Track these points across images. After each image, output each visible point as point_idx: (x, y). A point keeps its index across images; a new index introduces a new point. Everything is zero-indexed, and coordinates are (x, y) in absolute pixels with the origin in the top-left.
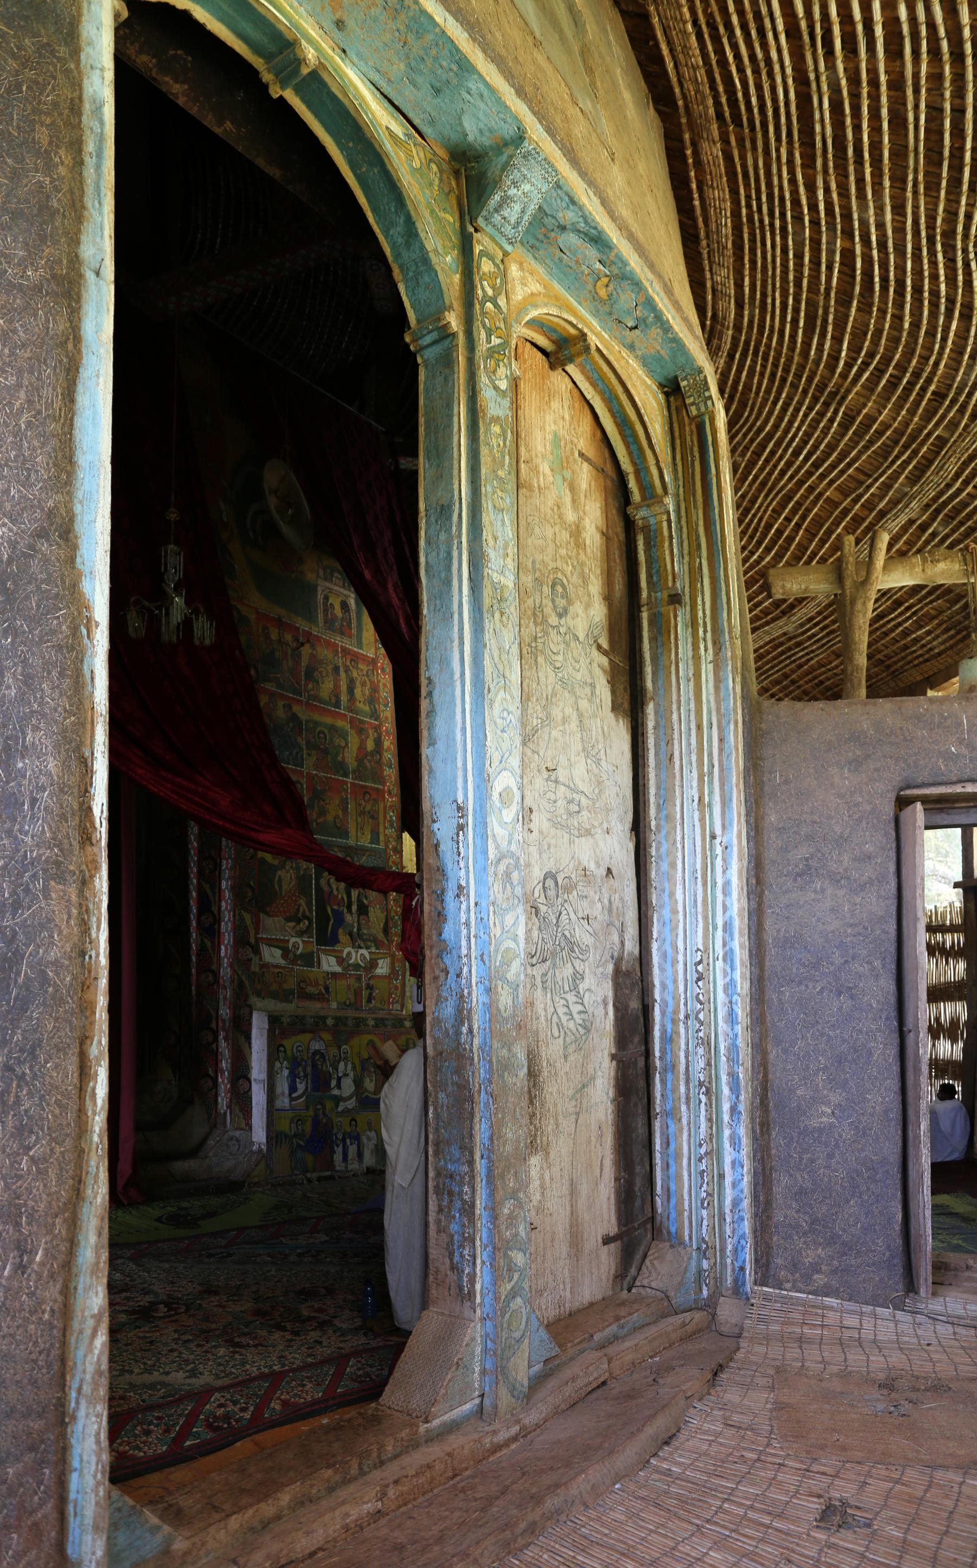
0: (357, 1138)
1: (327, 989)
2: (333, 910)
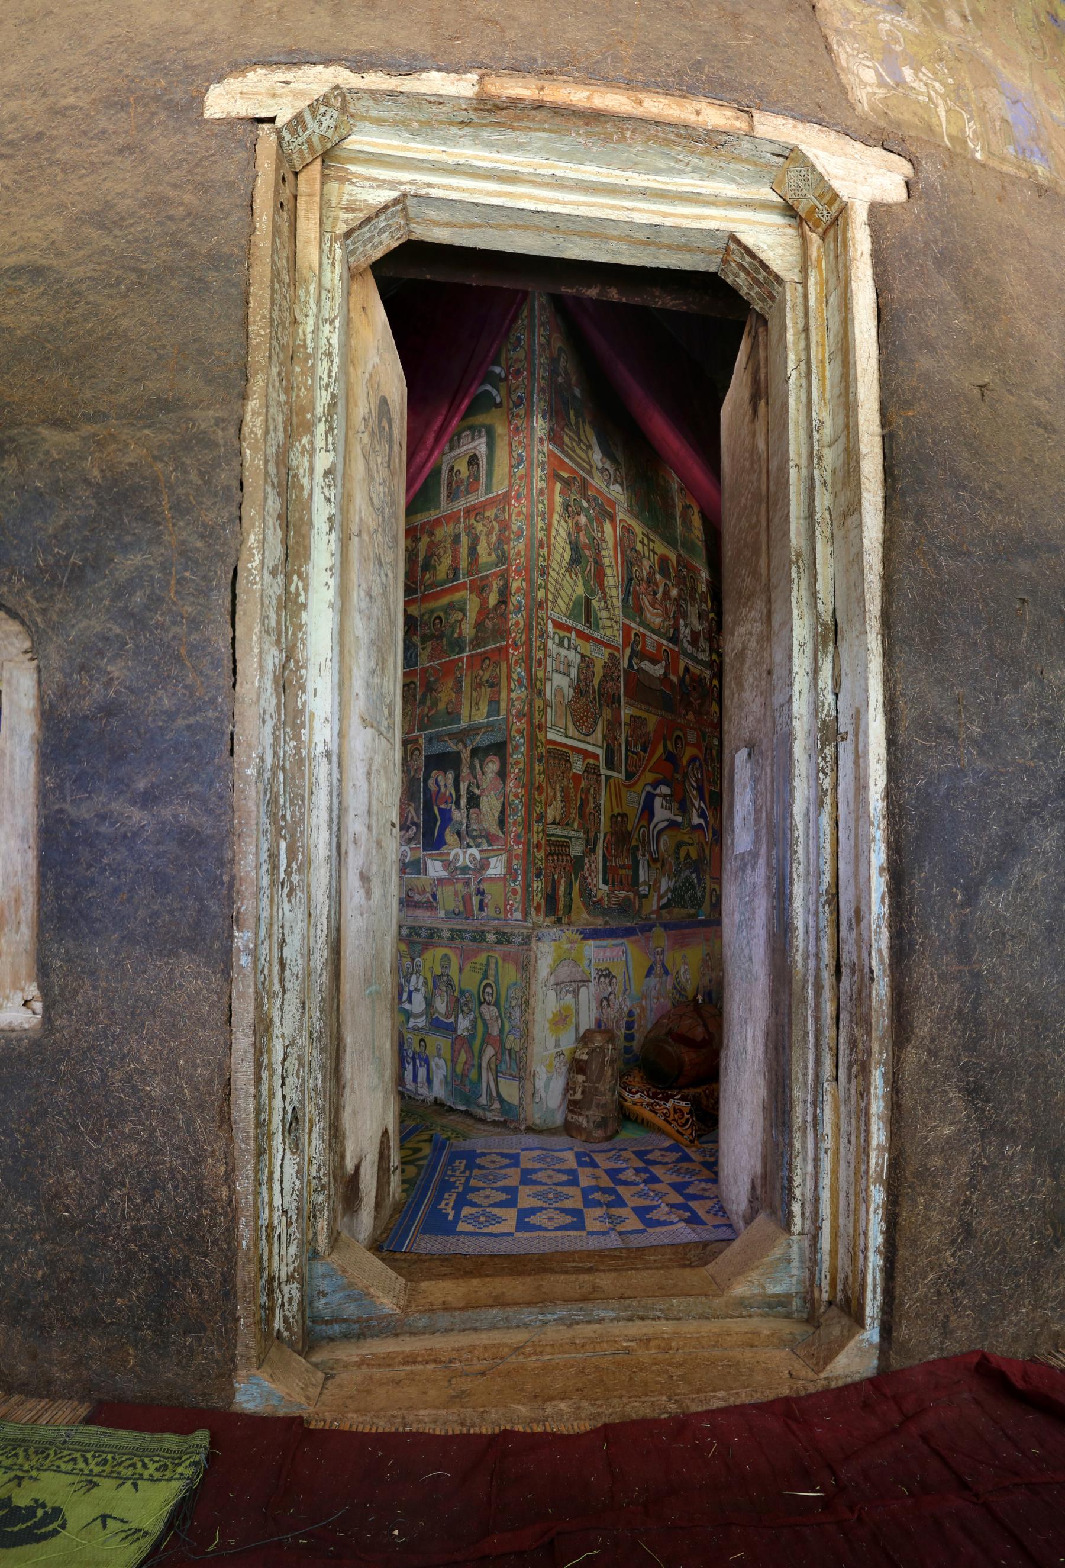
0: (426, 1061)
1: (434, 896)
2: (440, 809)
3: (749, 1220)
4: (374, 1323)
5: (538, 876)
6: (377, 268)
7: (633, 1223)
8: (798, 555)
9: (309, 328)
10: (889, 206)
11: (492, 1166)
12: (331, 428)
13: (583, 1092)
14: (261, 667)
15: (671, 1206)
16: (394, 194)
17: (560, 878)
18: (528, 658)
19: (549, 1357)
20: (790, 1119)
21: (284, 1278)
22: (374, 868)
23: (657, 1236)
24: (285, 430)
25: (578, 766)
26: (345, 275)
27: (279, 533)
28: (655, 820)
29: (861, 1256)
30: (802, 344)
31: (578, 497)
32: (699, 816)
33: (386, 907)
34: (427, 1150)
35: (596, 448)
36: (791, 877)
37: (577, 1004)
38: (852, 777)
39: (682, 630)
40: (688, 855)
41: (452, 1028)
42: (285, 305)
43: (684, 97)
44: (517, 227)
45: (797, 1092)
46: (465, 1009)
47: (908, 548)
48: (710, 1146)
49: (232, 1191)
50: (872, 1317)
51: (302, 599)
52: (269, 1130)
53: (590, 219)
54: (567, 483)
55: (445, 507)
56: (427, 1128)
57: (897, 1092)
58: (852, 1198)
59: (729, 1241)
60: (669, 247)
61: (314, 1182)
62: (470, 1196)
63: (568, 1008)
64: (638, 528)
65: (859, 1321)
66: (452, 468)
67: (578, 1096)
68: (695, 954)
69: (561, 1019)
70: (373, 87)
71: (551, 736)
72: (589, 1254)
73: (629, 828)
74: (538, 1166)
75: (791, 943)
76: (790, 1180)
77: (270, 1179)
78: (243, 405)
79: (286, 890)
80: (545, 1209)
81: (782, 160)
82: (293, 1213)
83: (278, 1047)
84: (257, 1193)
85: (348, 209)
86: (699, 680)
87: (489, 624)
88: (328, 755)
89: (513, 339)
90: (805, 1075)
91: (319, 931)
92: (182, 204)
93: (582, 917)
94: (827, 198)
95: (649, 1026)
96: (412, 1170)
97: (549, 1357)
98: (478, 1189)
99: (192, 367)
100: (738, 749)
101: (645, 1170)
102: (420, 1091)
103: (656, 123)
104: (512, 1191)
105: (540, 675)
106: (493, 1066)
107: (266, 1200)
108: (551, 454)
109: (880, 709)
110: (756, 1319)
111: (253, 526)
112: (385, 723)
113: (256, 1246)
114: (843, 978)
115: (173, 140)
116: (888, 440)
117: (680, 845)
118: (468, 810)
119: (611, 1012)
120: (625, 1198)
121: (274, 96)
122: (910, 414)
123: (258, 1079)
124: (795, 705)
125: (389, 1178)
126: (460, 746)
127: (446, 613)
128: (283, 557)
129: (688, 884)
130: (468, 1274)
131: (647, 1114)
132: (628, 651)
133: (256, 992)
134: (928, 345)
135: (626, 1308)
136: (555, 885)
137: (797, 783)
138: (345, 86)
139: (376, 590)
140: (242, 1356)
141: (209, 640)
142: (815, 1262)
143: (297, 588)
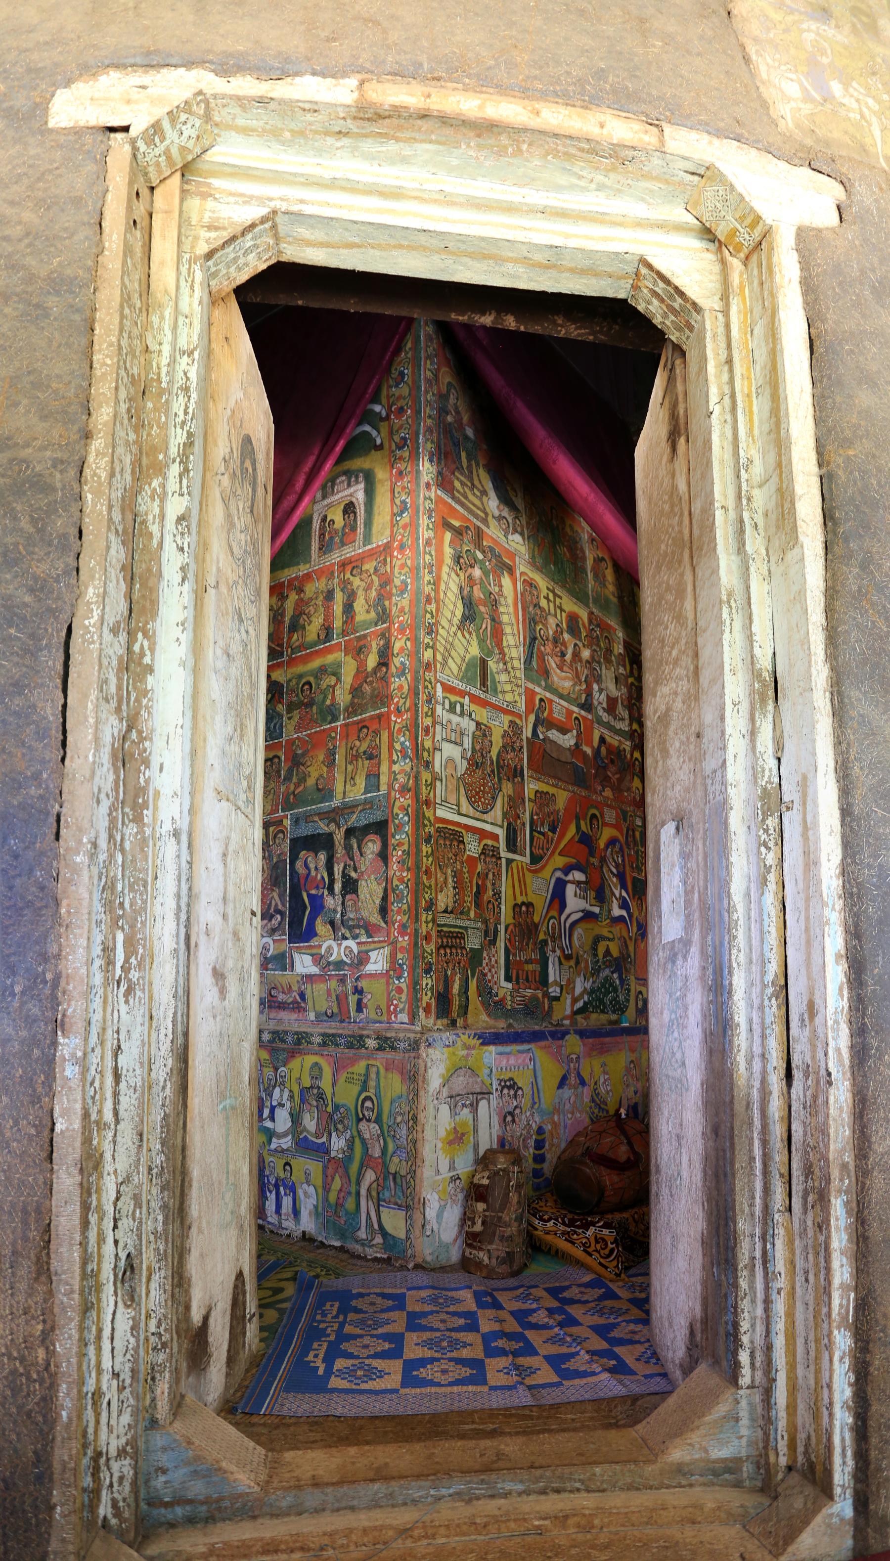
0: (293, 1189)
1: (302, 995)
2: (309, 895)
3: (688, 1369)
4: (227, 1503)
5: (428, 971)
6: (240, 291)
7: (546, 1375)
8: (730, 594)
9: (165, 361)
10: (820, 230)
11: (372, 1309)
12: (187, 470)
13: (483, 1223)
14: (97, 739)
15: (592, 1353)
16: (263, 211)
17: (454, 974)
18: (413, 728)
19: (444, 1540)
20: (735, 1256)
21: (113, 1452)
22: (230, 963)
23: (574, 1390)
24: (133, 472)
25: (473, 848)
26: (206, 299)
27: (123, 586)
28: (567, 911)
29: (825, 1413)
30: (725, 377)
31: (471, 547)
32: (621, 907)
33: (244, 1009)
34: (290, 1290)
35: (492, 494)
36: (730, 966)
37: (475, 1119)
38: (801, 851)
39: (596, 695)
40: (608, 952)
41: (323, 1150)
42: (136, 332)
43: (587, 108)
44: (401, 247)
45: (742, 1225)
46: (340, 1127)
47: (854, 597)
48: (640, 1279)
49: (51, 1353)
50: (843, 1486)
51: (147, 660)
52: (97, 1282)
53: (483, 239)
54: (458, 532)
55: (316, 560)
56: (291, 1265)
57: (863, 1223)
58: (812, 1345)
59: (665, 1394)
60: (572, 270)
61: (153, 1339)
62: (344, 1346)
63: (464, 1124)
64: (542, 582)
65: (826, 1491)
66: (325, 517)
67: (478, 1227)
68: (619, 1061)
69: (457, 1138)
70: (241, 93)
71: (441, 813)
72: (492, 1414)
73: (536, 919)
74: (427, 1308)
75: (731, 1042)
76: (736, 1325)
77: (99, 1337)
78: (86, 445)
79: (122, 989)
80: (438, 1360)
81: (696, 178)
82: (126, 1376)
83: (110, 1186)
84: (82, 1355)
85: (210, 228)
86: (616, 754)
87: (367, 688)
88: (176, 834)
89: (395, 374)
90: (752, 1205)
91: (162, 1037)
92: (20, 223)
93: (480, 1018)
94: (748, 221)
95: (563, 1145)
96: (272, 1315)
97: (444, 1540)
98: (355, 1337)
99: (25, 401)
100: (663, 824)
101: (561, 1311)
102: (285, 1224)
103: (556, 135)
104: (397, 1340)
105: (428, 744)
106: (374, 1194)
107: (93, 1362)
108: (439, 500)
109: (832, 776)
110: (698, 1489)
111: (92, 578)
112: (243, 797)
113: (80, 1417)
114: (795, 1083)
115: (12, 152)
116: (826, 481)
117: (597, 939)
118: (343, 896)
119: (517, 1130)
120: (535, 1344)
121: (128, 102)
122: (851, 453)
123: (85, 1224)
124: (730, 770)
125: (244, 1328)
126: (333, 826)
127: (316, 677)
128: (126, 613)
129: (608, 986)
130: (345, 1441)
131: (562, 1244)
132: (532, 718)
133: (84, 1108)
134: (869, 380)
135: (537, 1480)
136: (447, 982)
137: (734, 858)
138: (208, 91)
139: (235, 648)
140: (55, 1553)
141: (34, 706)
142: (768, 1421)
143: (142, 646)
